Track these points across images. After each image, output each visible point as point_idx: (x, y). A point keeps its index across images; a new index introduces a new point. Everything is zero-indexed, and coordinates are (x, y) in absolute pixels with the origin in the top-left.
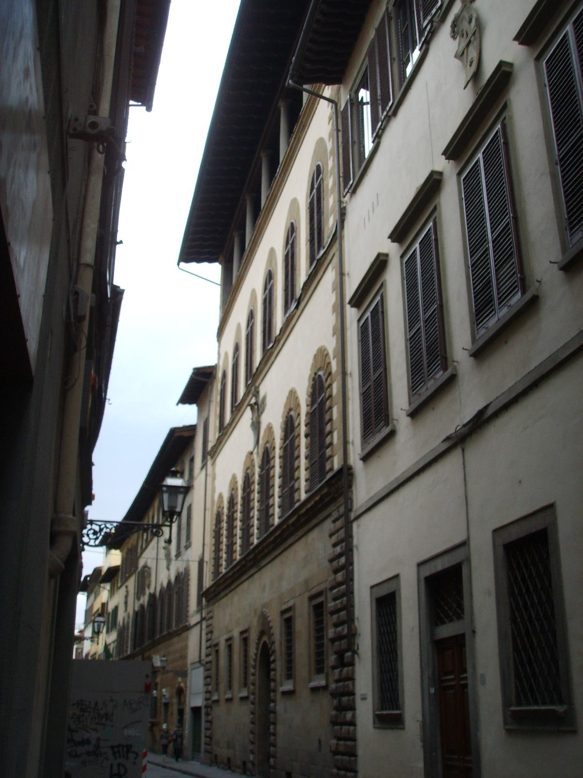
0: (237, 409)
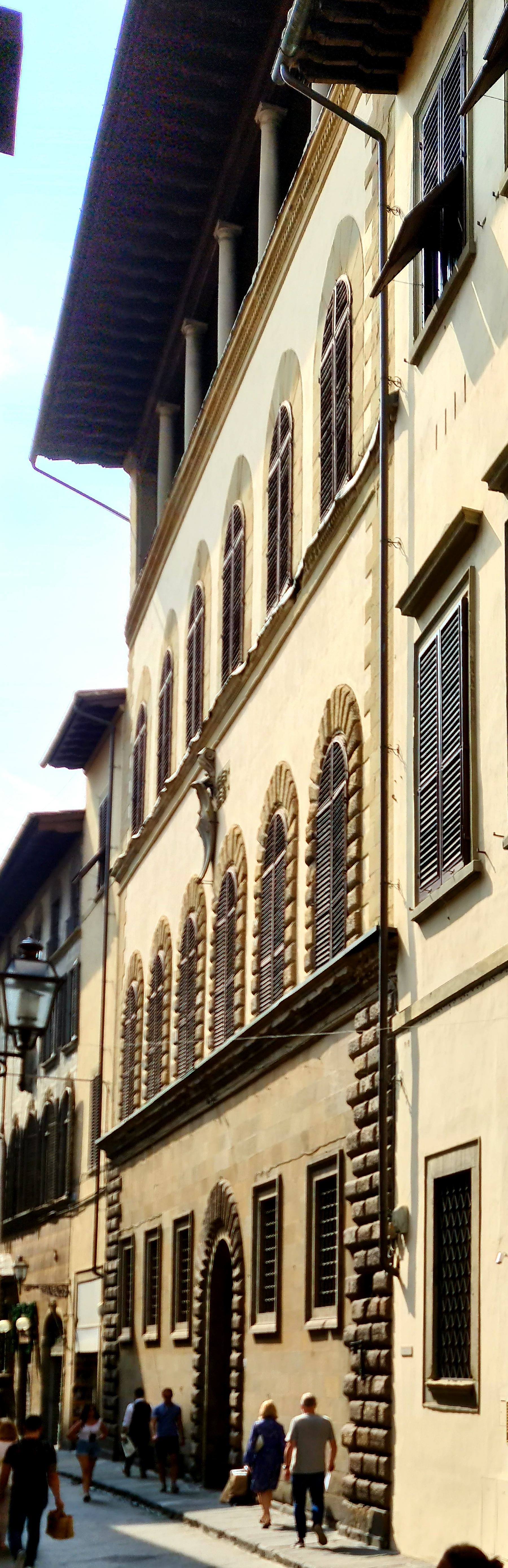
0: (170, 792)
